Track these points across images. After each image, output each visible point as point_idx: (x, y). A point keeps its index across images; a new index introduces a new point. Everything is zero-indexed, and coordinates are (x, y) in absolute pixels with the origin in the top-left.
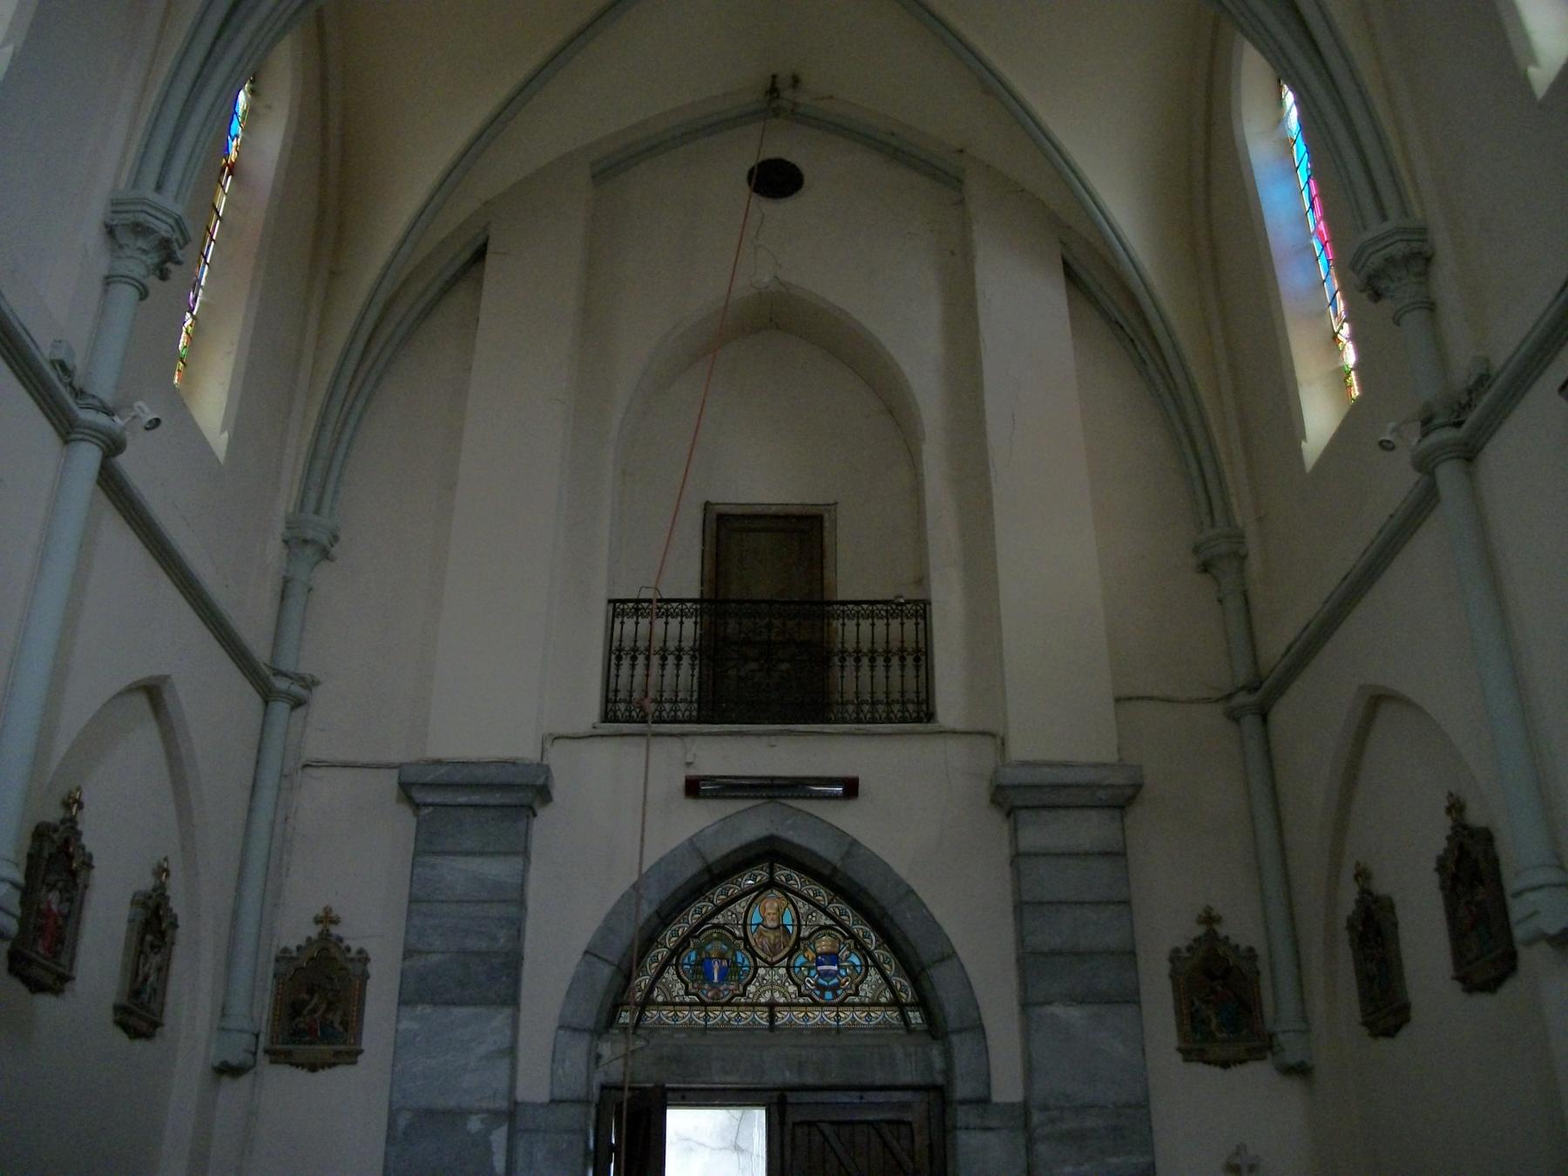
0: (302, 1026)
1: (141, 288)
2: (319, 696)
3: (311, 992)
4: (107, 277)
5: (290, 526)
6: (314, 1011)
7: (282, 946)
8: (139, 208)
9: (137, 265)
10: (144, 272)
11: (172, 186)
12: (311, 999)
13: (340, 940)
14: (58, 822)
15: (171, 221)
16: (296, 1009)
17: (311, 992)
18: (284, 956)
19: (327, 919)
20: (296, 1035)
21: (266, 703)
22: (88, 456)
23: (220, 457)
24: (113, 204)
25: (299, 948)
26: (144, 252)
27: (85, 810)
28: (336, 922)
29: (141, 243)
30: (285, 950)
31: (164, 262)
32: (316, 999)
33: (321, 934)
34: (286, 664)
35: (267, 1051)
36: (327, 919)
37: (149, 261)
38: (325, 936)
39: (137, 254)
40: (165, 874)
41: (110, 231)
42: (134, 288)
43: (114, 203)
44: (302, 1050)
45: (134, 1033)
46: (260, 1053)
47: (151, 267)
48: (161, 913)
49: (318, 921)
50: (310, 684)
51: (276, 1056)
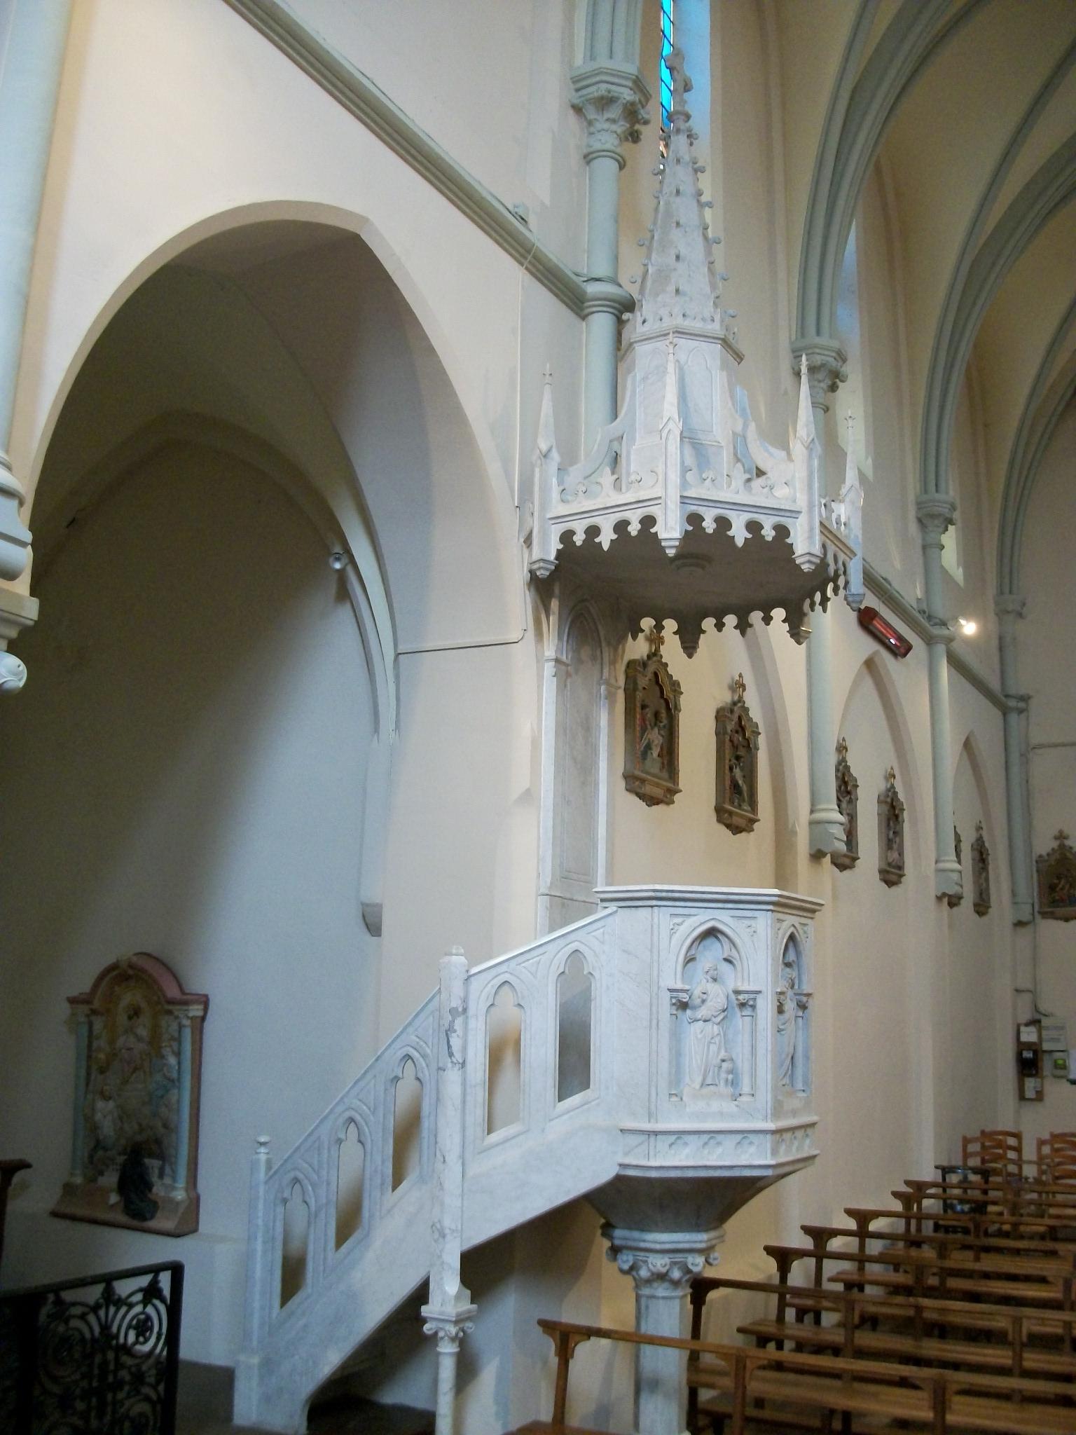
0: (1057, 898)
1: (619, 158)
2: (1033, 703)
3: (1059, 878)
4: (585, 157)
5: (997, 604)
6: (1062, 889)
7: (1038, 854)
8: (598, 79)
9: (608, 136)
10: (616, 142)
11: (619, 47)
12: (1059, 883)
13: (1071, 848)
14: (645, 658)
15: (834, 354)
16: (1052, 888)
17: (1059, 878)
18: (1040, 860)
19: (1061, 836)
20: (1054, 903)
21: (1005, 714)
22: (941, 649)
23: (870, 478)
24: (574, 82)
25: (1048, 855)
26: (614, 121)
27: (848, 752)
28: (1066, 838)
29: (936, 522)
30: (1041, 856)
31: (632, 125)
32: (1063, 882)
33: (1060, 846)
34: (1012, 691)
35: (1039, 912)
36: (1061, 836)
37: (619, 131)
38: (1062, 846)
39: (606, 126)
40: (741, 689)
41: (920, 520)
42: (614, 161)
43: (575, 80)
44: (1060, 911)
45: (890, 883)
46: (1036, 914)
47: (622, 136)
48: (846, 779)
49: (1056, 838)
50: (1025, 699)
51: (1044, 915)
